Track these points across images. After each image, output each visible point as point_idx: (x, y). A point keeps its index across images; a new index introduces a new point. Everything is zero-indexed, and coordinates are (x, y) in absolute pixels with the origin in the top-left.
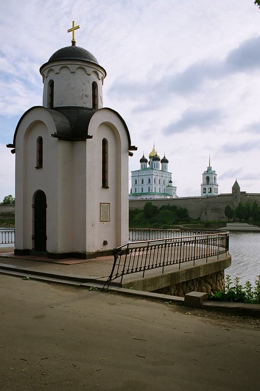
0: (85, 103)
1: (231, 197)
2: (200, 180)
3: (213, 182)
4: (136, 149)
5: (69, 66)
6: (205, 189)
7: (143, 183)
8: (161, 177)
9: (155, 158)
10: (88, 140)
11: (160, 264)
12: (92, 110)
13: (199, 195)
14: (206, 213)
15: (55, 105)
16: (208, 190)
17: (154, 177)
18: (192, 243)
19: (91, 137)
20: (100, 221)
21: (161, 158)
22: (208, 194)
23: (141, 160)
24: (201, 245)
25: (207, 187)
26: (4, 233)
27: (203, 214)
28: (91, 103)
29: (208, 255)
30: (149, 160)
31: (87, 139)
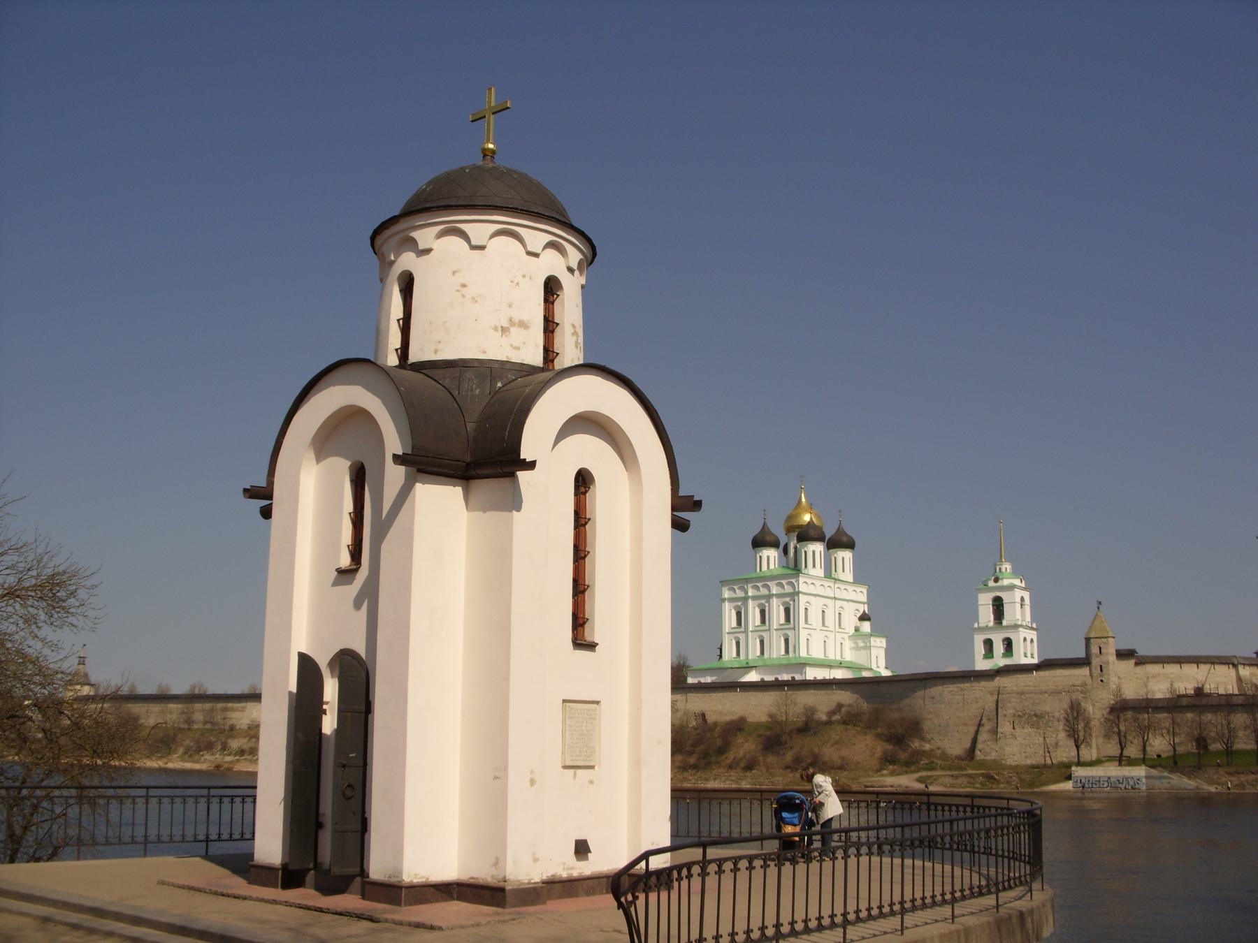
0: (517, 348)
1: (1085, 671)
3: (1018, 616)
4: (697, 505)
5: (462, 226)
10: (522, 475)
12: (542, 370)
14: (994, 731)
15: (415, 356)
16: (999, 648)
18: (870, 854)
19: (531, 465)
21: (829, 533)
24: (875, 859)
26: (190, 801)
27: (983, 737)
28: (537, 346)
29: (908, 905)
31: (518, 473)
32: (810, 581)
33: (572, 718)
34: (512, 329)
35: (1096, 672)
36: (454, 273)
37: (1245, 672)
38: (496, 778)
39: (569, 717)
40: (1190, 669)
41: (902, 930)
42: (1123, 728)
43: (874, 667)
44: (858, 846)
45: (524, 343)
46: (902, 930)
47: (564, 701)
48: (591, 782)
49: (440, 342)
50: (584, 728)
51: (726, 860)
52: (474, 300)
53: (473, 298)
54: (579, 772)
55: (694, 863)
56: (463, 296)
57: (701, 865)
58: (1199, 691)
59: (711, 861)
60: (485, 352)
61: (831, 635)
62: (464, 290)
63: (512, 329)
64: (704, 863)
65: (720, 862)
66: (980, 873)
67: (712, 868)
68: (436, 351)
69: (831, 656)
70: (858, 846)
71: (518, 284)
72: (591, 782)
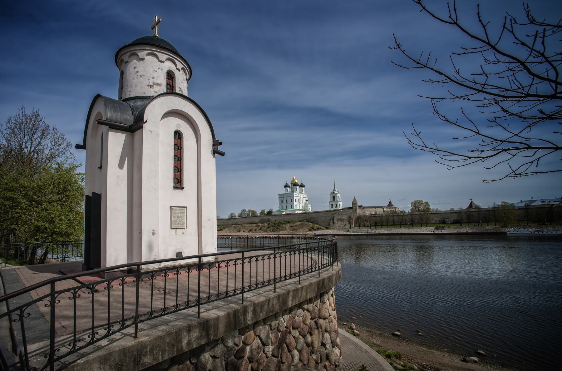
2: (329, 198)
3: (338, 199)
6: (332, 205)
7: (287, 202)
8: (300, 198)
9: (295, 184)
11: (280, 256)
13: (328, 209)
16: (334, 206)
17: (295, 197)
20: (171, 228)
22: (334, 208)
23: (285, 186)
25: (334, 204)
30: (291, 186)
32: (296, 194)
33: (174, 212)
34: (154, 86)
35: (354, 210)
36: (134, 68)
37: (385, 209)
38: (140, 233)
39: (173, 212)
40: (374, 209)
41: (275, 290)
42: (360, 221)
43: (309, 210)
44: (299, 250)
45: (159, 91)
46: (275, 290)
47: (171, 207)
48: (184, 233)
49: (130, 91)
50: (180, 215)
51: (265, 255)
52: (141, 76)
53: (141, 76)
54: (178, 230)
55: (238, 259)
56: (137, 75)
57: (242, 260)
58: (375, 214)
59: (246, 258)
60: (145, 94)
61: (300, 204)
62: (138, 74)
63: (154, 86)
64: (243, 259)
65: (250, 258)
66: (330, 254)
67: (247, 261)
68: (129, 95)
69: (300, 208)
70: (299, 250)
71: (156, 71)
72: (184, 233)
